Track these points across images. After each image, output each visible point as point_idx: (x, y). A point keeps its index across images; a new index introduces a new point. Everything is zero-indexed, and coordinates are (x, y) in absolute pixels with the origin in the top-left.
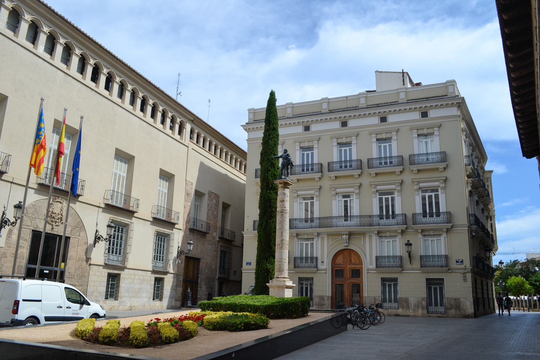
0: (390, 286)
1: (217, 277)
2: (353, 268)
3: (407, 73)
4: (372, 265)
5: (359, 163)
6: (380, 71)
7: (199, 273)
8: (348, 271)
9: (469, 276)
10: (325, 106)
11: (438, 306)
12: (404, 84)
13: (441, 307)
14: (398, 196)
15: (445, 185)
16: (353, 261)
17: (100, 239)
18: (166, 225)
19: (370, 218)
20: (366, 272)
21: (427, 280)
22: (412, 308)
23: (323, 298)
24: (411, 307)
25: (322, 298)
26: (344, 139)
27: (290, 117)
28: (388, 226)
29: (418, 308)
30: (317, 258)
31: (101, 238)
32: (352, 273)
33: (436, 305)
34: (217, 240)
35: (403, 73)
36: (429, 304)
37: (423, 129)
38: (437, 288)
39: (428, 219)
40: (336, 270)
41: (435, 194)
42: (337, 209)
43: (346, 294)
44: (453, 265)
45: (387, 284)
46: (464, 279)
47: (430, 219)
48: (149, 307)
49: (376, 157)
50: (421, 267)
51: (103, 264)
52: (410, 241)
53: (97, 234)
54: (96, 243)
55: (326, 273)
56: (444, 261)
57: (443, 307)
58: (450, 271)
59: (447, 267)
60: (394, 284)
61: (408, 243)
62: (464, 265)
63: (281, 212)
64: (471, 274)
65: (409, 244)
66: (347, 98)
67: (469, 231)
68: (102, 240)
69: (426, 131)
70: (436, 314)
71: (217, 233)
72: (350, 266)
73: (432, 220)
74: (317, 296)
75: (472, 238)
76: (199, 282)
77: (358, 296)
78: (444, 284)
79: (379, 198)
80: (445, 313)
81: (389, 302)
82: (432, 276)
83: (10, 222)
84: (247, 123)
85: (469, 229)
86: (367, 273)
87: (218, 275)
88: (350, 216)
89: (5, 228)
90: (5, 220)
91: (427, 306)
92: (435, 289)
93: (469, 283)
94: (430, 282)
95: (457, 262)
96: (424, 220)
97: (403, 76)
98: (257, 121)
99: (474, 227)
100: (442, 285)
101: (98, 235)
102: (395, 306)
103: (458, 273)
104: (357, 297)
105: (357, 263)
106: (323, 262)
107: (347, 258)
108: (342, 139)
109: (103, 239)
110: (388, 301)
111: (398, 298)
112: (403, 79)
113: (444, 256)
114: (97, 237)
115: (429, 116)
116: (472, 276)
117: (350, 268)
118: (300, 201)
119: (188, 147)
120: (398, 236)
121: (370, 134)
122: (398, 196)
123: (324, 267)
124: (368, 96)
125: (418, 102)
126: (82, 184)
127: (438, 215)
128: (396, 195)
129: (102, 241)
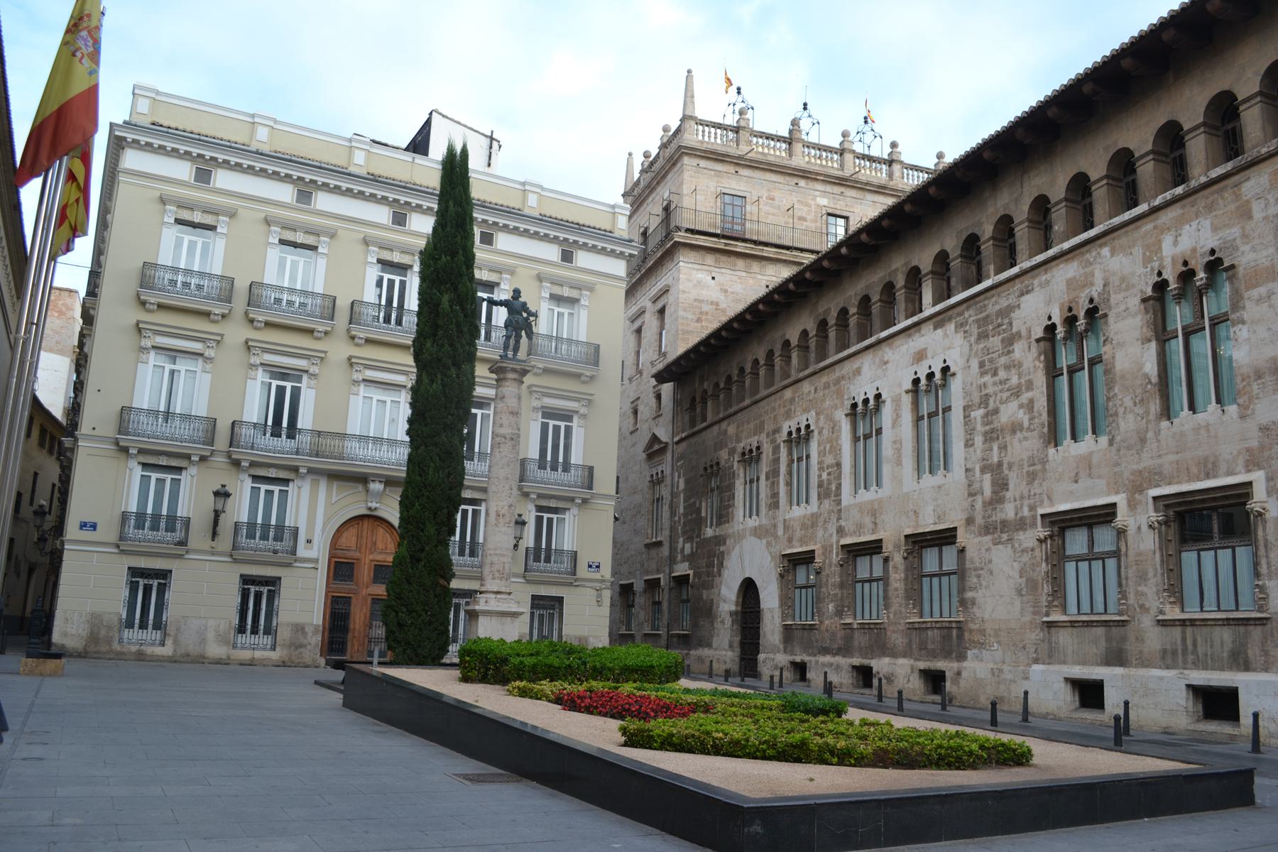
2: (378, 561)
5: (328, 303)
12: (489, 165)
21: (534, 597)
23: (303, 629)
25: (299, 629)
30: (295, 532)
32: (375, 573)
35: (492, 138)
39: (548, 474)
40: (336, 562)
41: (292, 386)
42: (254, 406)
43: (357, 621)
44: (583, 571)
52: (227, 488)
56: (181, 531)
60: (159, 584)
63: (512, 439)
72: (371, 557)
73: (273, 443)
74: (288, 625)
79: (542, 422)
81: (154, 629)
88: (479, 453)
94: (537, 602)
95: (590, 566)
96: (540, 474)
97: (491, 147)
98: (161, 126)
106: (309, 541)
117: (372, 561)
121: (366, 242)
123: (312, 554)
124: (372, 150)
125: (544, 221)
128: (575, 423)
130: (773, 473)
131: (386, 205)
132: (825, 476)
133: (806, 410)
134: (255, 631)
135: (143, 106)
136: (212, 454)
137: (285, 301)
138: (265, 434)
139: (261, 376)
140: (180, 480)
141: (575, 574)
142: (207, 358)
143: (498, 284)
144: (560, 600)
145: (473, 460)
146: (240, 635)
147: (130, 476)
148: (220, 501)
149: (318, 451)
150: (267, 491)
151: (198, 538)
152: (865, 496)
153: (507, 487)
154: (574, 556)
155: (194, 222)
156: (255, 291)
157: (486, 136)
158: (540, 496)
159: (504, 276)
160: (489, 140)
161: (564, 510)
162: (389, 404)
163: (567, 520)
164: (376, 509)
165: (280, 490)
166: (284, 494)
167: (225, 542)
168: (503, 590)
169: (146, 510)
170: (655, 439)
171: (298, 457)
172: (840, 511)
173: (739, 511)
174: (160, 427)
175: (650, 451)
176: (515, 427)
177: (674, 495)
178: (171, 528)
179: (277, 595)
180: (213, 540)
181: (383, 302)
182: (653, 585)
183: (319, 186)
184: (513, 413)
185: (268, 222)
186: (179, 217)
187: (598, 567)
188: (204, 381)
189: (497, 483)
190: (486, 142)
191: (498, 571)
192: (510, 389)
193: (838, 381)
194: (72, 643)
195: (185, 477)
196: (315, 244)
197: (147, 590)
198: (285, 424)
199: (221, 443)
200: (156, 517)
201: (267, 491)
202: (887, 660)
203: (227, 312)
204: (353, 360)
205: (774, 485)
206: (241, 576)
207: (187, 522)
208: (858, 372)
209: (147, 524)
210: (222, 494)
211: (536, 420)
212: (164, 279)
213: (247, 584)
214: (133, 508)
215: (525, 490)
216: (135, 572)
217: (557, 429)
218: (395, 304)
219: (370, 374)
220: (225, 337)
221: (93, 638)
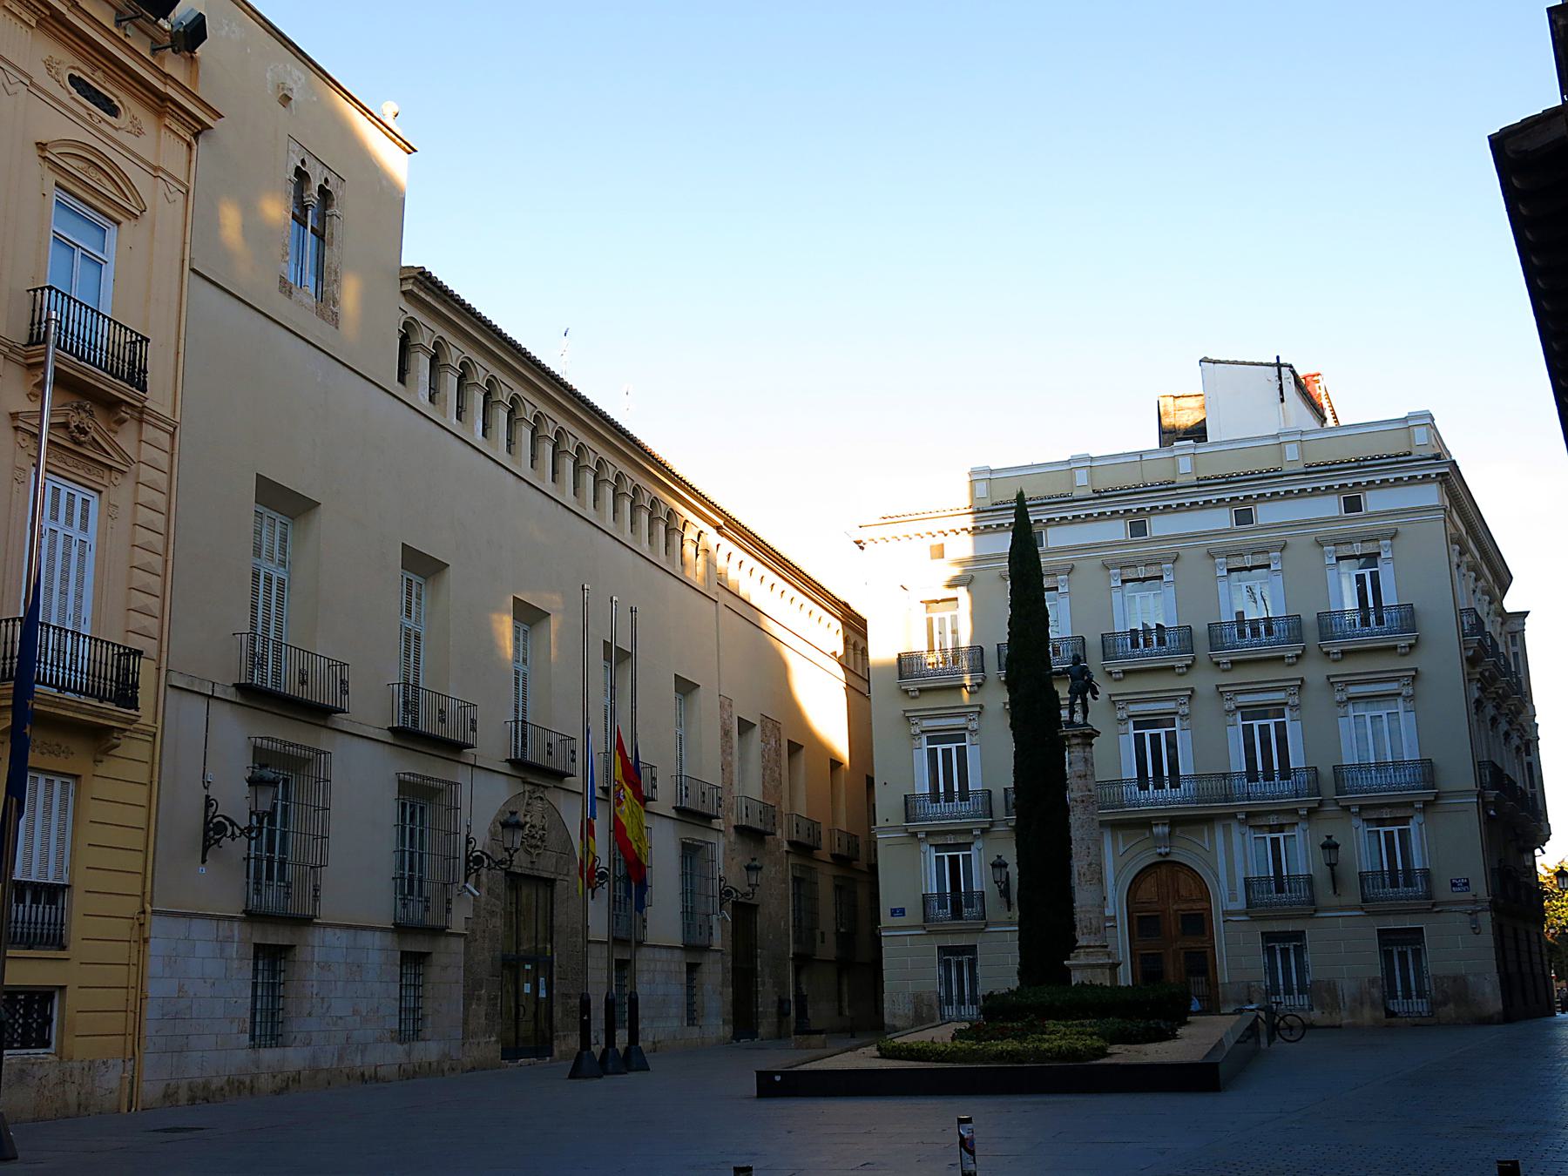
0: (1285, 952)
1: (791, 952)
3: (1291, 366)
4: (1236, 901)
6: (1215, 358)
7: (758, 945)
8: (1172, 918)
9: (1486, 919)
10: (1081, 478)
11: (1411, 998)
13: (1419, 1000)
15: (1299, 698)
16: (1183, 892)
17: (226, 829)
18: (703, 824)
19: (1225, 779)
22: (1348, 1004)
24: (1344, 1003)
27: (985, 509)
29: (1362, 1004)
31: (230, 828)
33: (1407, 995)
34: (785, 849)
35: (1279, 365)
37: (1351, 543)
38: (1406, 952)
39: (943, 807)
40: (1139, 917)
44: (1443, 892)
45: (1277, 947)
46: (1474, 926)
48: (683, 1041)
50: (1364, 900)
51: (236, 910)
52: (1333, 839)
53: (211, 814)
54: (210, 846)
55: (1116, 927)
57: (1424, 1000)
58: (1437, 909)
59: (1431, 899)
60: (1295, 946)
61: (1330, 842)
62: (1472, 892)
63: (1083, 801)
64: (1491, 915)
65: (1330, 846)
66: (1141, 458)
67: (1481, 806)
68: (233, 833)
70: (1408, 1019)
72: (1175, 907)
75: (1489, 823)
76: (759, 968)
77: (1202, 982)
78: (1424, 942)
80: (1430, 1014)
83: (238, 828)
85: (1480, 801)
86: (1224, 922)
87: (794, 948)
89: (221, 847)
90: (215, 820)
91: (1384, 1000)
92: (1403, 956)
93: (1487, 938)
94: (1387, 938)
95: (1454, 885)
97: (1280, 378)
99: (1492, 794)
100: (1419, 944)
101: (473, 852)
103: (1457, 914)
104: (1200, 986)
105: (1194, 898)
107: (1168, 886)
109: (237, 832)
110: (1296, 991)
111: (1308, 982)
112: (1281, 385)
113: (1420, 873)
114: (471, 858)
116: (1493, 919)
119: (716, 602)
120: (1300, 825)
126: (305, 687)
129: (233, 839)
135: (982, 489)
141: (984, 917)
147: (925, 857)
149: (1226, 795)
151: (1325, 895)
162: (1385, 717)
164: (1167, 854)
174: (1375, 779)
176: (1084, 788)
180: (1009, 910)
184: (1079, 777)
185: (1320, 544)
187: (1466, 884)
188: (1407, 722)
191: (1086, 927)
195: (1412, 826)
197: (960, 965)
199: (1329, 791)
203: (1414, 641)
217: (947, 752)
219: (1354, 690)
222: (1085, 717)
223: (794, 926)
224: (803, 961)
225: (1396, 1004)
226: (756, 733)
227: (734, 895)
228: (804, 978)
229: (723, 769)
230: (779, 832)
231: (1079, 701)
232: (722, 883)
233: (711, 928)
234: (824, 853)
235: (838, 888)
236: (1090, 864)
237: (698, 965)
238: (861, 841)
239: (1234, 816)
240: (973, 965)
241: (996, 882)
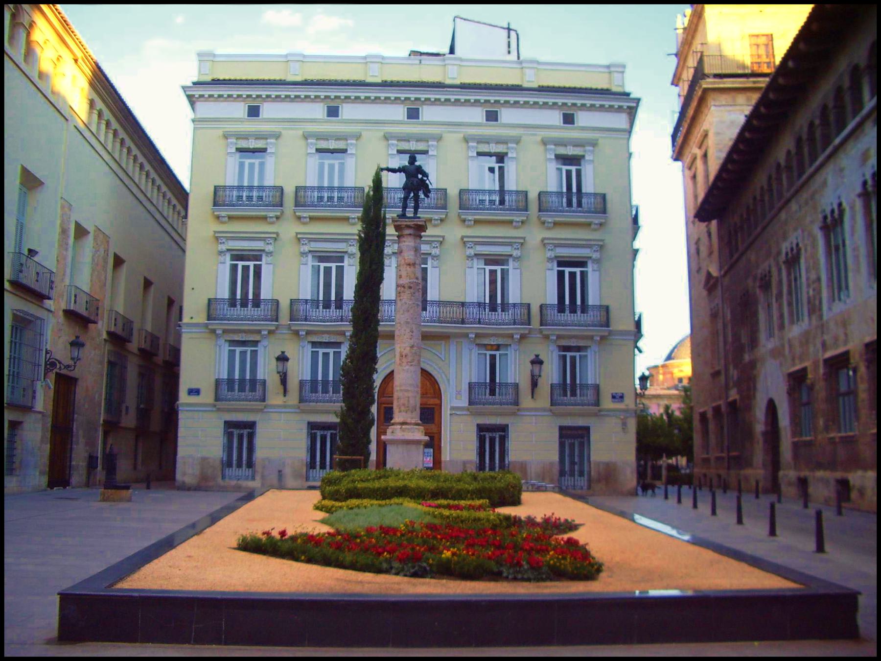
14: (594, 270)
19: (463, 307)
20: (449, 412)
21: (561, 428)
26: (413, 144)
28: (253, 321)
35: (509, 29)
36: (562, 473)
40: (385, 407)
41: (255, 265)
44: (607, 403)
47: (492, 314)
49: (354, 186)
63: (410, 288)
66: (420, 62)
69: (413, 146)
71: (103, 321)
76: (74, 430)
82: (568, 422)
84: (194, 84)
94: (565, 433)
95: (614, 397)
97: (509, 37)
102: (230, 474)
108: (247, 141)
115: (342, 116)
118: (478, 265)
120: (512, 346)
122: (594, 270)
127: (584, 308)
128: (590, 269)
130: (780, 295)
131: (479, 106)
132: (811, 292)
133: (795, 229)
134: (239, 465)
136: (277, 328)
137: (487, 201)
138: (318, 308)
139: (310, 261)
140: (340, 352)
142: (435, 256)
143: (583, 157)
144: (587, 429)
145: (496, 311)
146: (311, 470)
148: (536, 368)
150: (324, 354)
152: (838, 307)
153: (408, 331)
154: (597, 388)
155: (330, 149)
156: (543, 199)
157: (504, 28)
158: (559, 337)
159: (510, 145)
160: (507, 31)
161: (585, 348)
163: (509, 355)
165: (334, 352)
166: (254, 354)
167: (293, 397)
168: (409, 421)
169: (245, 377)
170: (709, 275)
171: (343, 323)
172: (822, 326)
173: (762, 336)
175: (709, 285)
176: (412, 276)
177: (725, 327)
178: (253, 389)
179: (506, 439)
180: (285, 396)
181: (565, 190)
182: (717, 410)
183: (264, 98)
184: (409, 265)
186: (239, 146)
189: (399, 328)
190: (505, 32)
191: (404, 405)
192: (407, 243)
193: (812, 197)
194: (189, 480)
196: (344, 147)
197: (241, 437)
198: (567, 302)
200: (242, 381)
201: (324, 354)
202: (860, 473)
204: (465, 239)
205: (780, 307)
206: (309, 423)
207: (516, 386)
208: (825, 183)
209: (247, 388)
210: (537, 361)
211: (552, 269)
212: (394, 198)
213: (483, 432)
214: (225, 376)
215: (545, 333)
216: (229, 425)
217: (572, 275)
218: (574, 190)
220: (526, 239)
221: (204, 477)
222: (416, 212)
223: (106, 399)
224: (111, 427)
225: (582, 481)
226: (89, 241)
227: (58, 367)
228: (110, 441)
229: (58, 261)
230: (100, 323)
231: (412, 195)
232: (48, 356)
233: (34, 392)
234: (133, 346)
235: (141, 375)
236: (412, 347)
237: (21, 423)
238: (161, 342)
239: (466, 335)
240: (251, 436)
241: (278, 372)
